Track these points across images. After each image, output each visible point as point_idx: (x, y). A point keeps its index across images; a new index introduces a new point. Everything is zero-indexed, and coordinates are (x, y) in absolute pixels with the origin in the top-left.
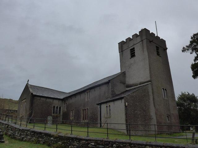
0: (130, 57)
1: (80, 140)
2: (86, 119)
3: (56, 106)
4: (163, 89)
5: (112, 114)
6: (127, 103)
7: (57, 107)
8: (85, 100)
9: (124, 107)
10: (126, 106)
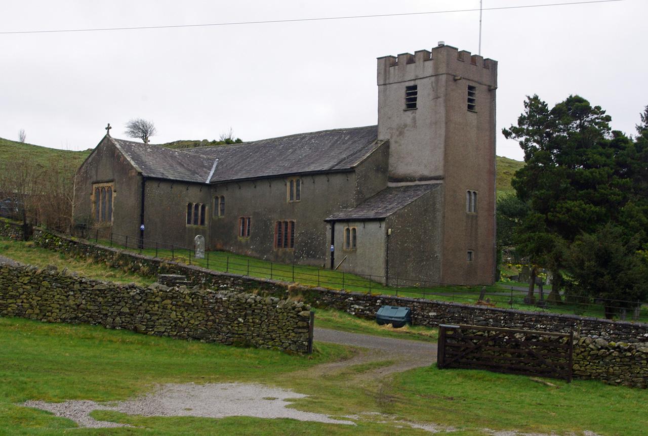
0: (404, 107)
1: (334, 294)
2: (286, 245)
3: (194, 204)
4: (469, 192)
5: (358, 245)
6: (390, 230)
7: (197, 206)
8: (285, 199)
9: (384, 236)
10: (388, 236)
